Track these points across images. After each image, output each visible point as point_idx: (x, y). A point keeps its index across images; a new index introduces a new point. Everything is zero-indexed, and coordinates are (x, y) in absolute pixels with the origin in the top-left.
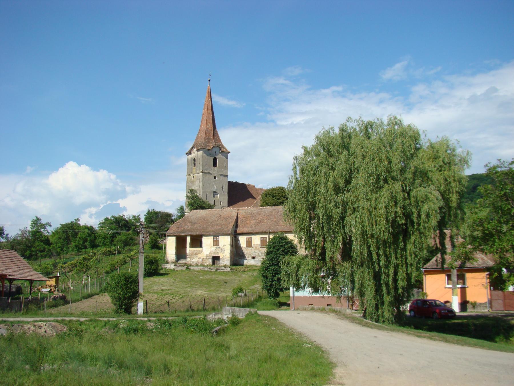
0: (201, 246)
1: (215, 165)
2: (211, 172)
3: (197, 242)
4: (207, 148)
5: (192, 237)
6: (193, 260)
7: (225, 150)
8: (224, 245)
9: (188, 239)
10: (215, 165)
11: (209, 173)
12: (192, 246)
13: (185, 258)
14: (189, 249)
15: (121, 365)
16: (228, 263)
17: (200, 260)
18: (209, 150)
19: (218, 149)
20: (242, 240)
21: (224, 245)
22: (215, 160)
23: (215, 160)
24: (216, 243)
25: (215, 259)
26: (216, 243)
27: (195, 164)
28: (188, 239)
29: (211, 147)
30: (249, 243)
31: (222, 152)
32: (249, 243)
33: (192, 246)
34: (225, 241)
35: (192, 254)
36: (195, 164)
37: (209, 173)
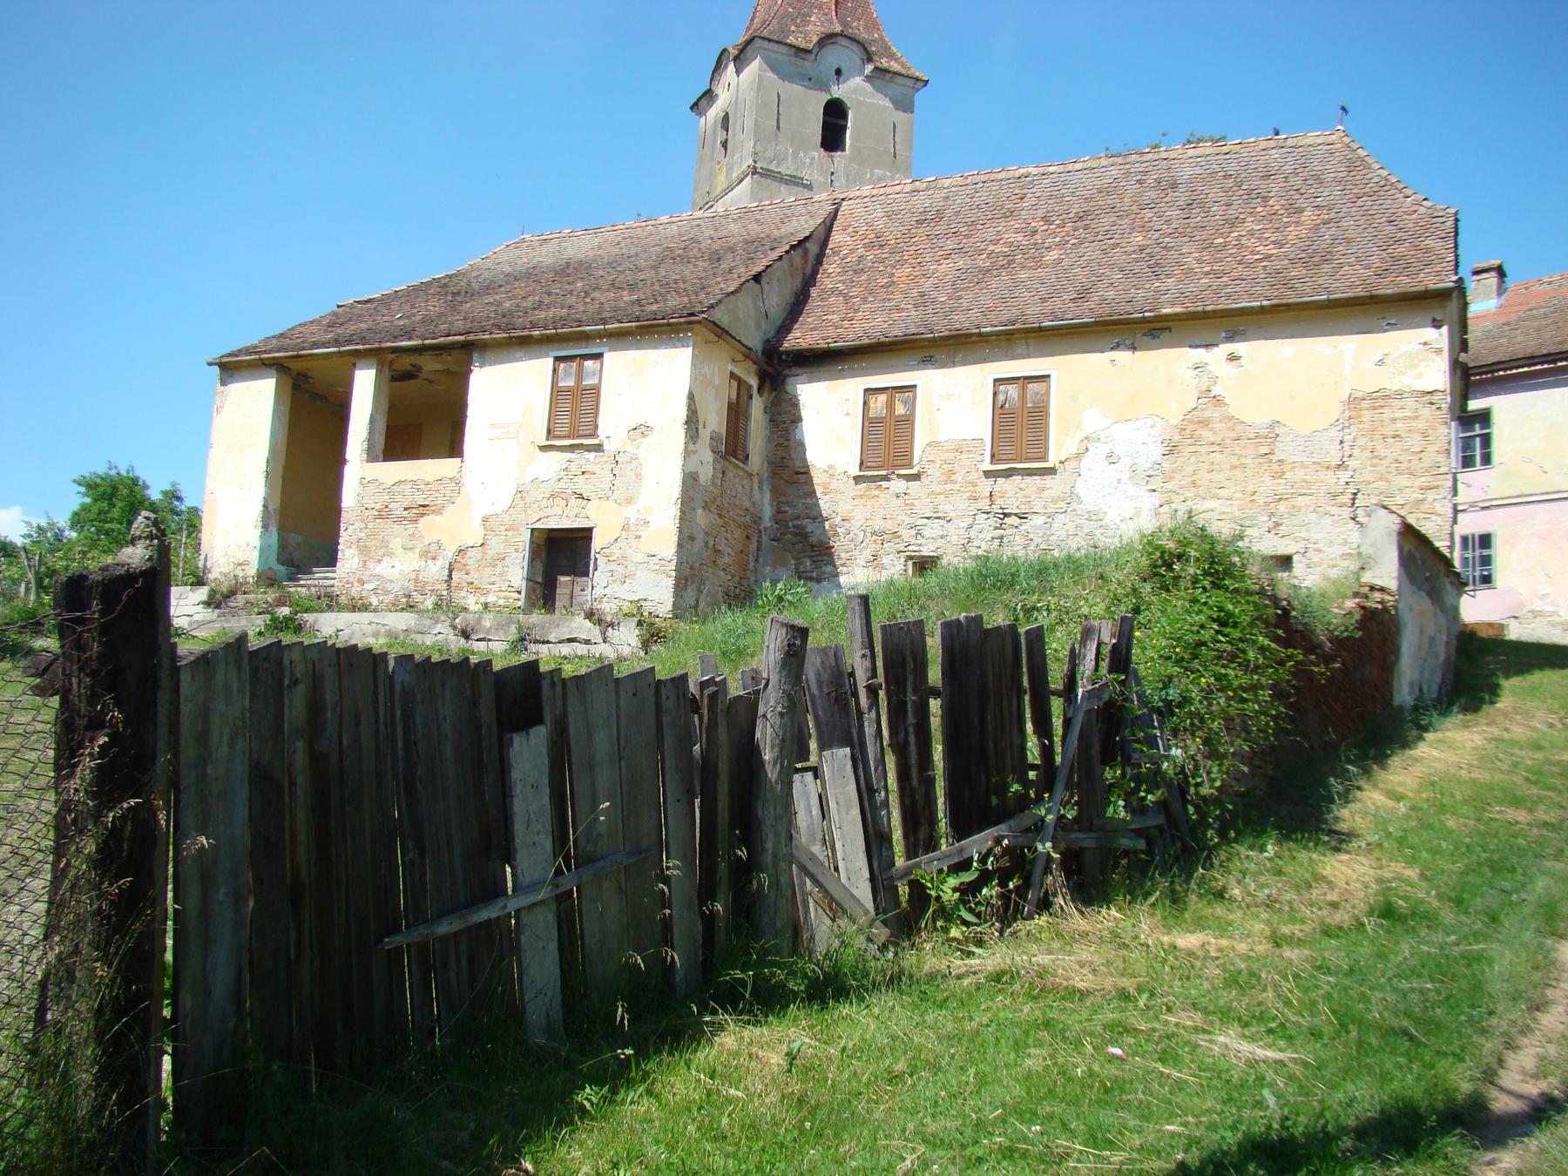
0: (453, 446)
1: (832, 138)
2: (806, 175)
3: (426, 420)
4: (791, 40)
5: (400, 373)
6: (383, 569)
7: (895, 66)
8: (641, 430)
9: (365, 384)
10: (832, 138)
11: (794, 181)
12: (372, 457)
13: (331, 560)
14: (363, 477)
15: (1240, 1019)
16: (659, 594)
17: (436, 570)
18: (800, 51)
19: (855, 54)
20: (829, 414)
21: (641, 430)
22: (835, 113)
23: (835, 113)
24: (573, 419)
25: (561, 555)
26: (573, 419)
27: (725, 145)
28: (365, 384)
29: (815, 39)
30: (887, 446)
31: (881, 72)
32: (887, 446)
33: (372, 457)
34: (653, 393)
35: (383, 514)
36: (725, 145)
37: (794, 181)
